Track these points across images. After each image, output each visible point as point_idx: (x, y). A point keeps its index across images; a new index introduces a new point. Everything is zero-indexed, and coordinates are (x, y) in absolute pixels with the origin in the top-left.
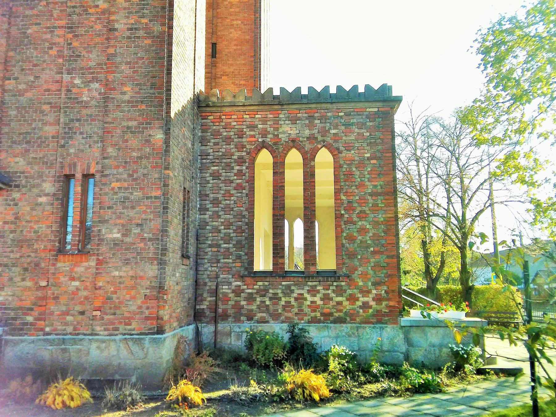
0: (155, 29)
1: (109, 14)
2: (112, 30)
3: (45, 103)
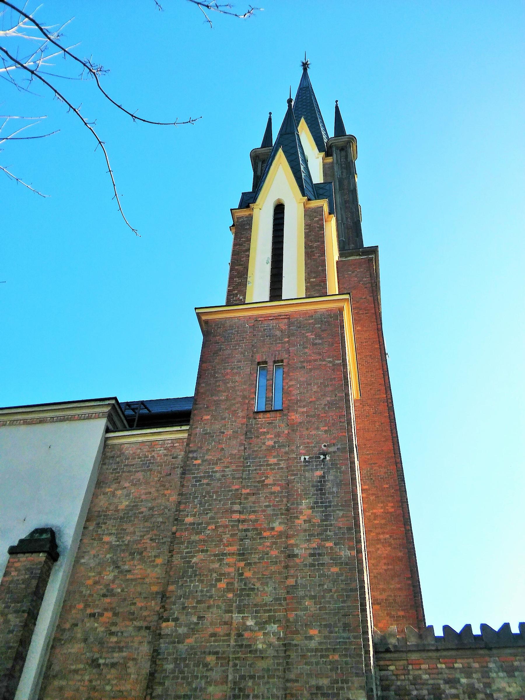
0: (342, 553)
1: (287, 537)
2: (292, 556)
3: (210, 653)
